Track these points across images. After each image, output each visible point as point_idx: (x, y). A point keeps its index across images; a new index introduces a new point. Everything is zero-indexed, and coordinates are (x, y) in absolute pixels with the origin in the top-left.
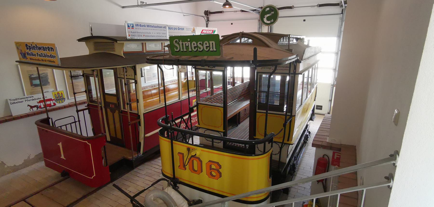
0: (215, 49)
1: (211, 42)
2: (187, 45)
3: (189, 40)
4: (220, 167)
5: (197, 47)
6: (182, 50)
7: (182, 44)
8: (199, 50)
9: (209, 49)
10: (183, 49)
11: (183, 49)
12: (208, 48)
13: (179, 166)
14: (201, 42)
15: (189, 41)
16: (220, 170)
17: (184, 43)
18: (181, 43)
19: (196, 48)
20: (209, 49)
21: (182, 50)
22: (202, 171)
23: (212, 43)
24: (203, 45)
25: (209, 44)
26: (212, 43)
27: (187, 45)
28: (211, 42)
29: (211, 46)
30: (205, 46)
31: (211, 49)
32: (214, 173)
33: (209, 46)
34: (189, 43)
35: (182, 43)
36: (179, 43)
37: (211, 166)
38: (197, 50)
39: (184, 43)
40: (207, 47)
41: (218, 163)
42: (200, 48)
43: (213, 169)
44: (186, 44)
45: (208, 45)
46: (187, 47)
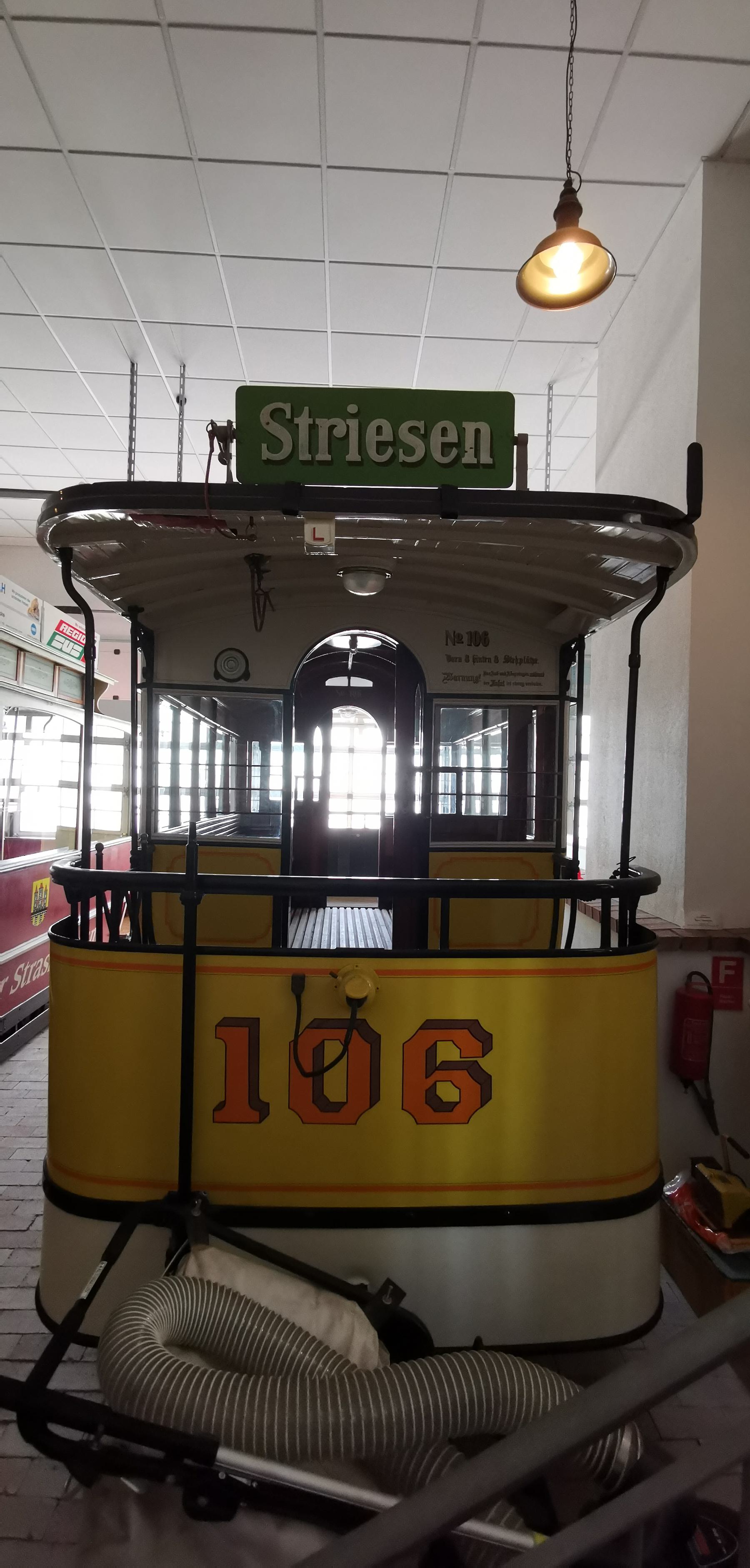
0: (485, 458)
1: (470, 427)
2: (339, 432)
3: (352, 409)
4: (486, 1041)
5: (395, 442)
6: (304, 456)
7: (313, 428)
8: (402, 457)
9: (458, 458)
10: (313, 447)
11: (313, 447)
12: (454, 452)
13: (221, 1106)
14: (421, 425)
15: (353, 416)
16: (486, 1063)
17: (323, 424)
18: (303, 421)
19: (390, 451)
20: (458, 458)
21: (304, 456)
22: (374, 1097)
23: (478, 431)
24: (425, 437)
25: (461, 433)
26: (478, 431)
27: (339, 432)
28: (470, 427)
29: (469, 442)
30: (436, 440)
31: (469, 458)
32: (448, 1092)
33: (460, 444)
34: (354, 424)
35: (311, 421)
36: (291, 421)
37: (432, 1051)
38: (394, 456)
39: (323, 424)
40: (446, 447)
41: (473, 1027)
42: (410, 451)
43: (448, 1066)
44: (332, 428)
45: (452, 437)
46: (338, 444)
